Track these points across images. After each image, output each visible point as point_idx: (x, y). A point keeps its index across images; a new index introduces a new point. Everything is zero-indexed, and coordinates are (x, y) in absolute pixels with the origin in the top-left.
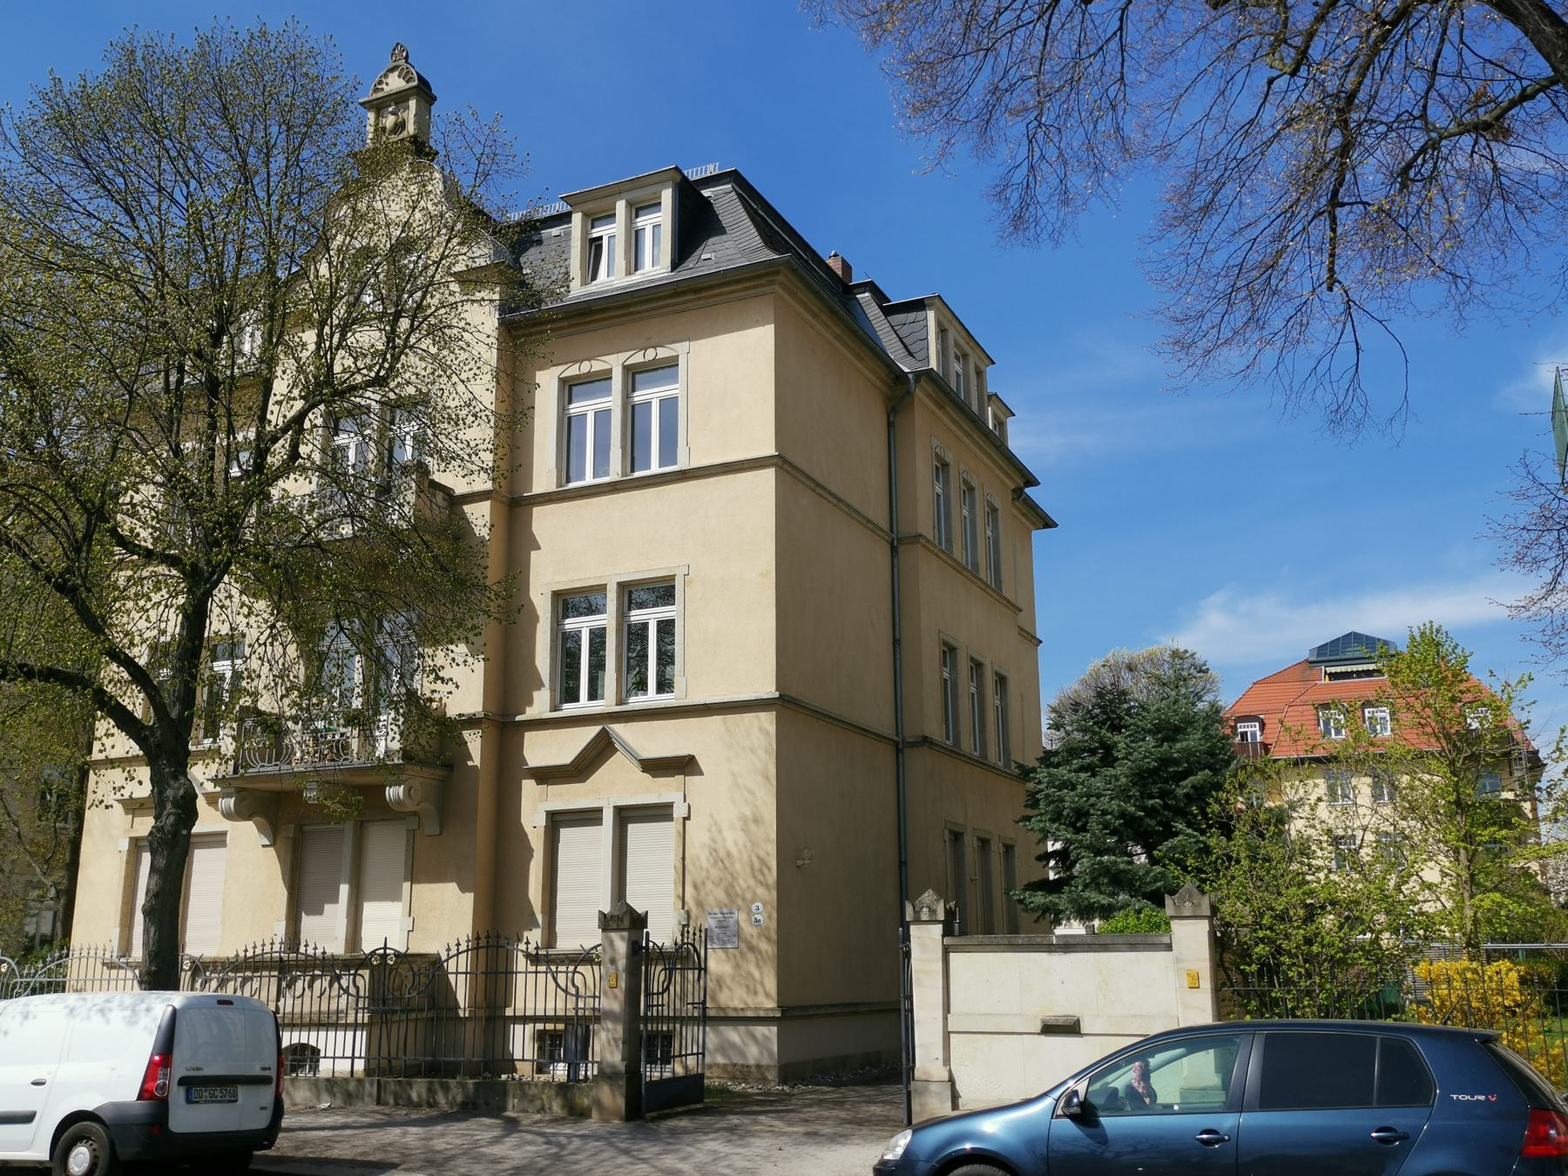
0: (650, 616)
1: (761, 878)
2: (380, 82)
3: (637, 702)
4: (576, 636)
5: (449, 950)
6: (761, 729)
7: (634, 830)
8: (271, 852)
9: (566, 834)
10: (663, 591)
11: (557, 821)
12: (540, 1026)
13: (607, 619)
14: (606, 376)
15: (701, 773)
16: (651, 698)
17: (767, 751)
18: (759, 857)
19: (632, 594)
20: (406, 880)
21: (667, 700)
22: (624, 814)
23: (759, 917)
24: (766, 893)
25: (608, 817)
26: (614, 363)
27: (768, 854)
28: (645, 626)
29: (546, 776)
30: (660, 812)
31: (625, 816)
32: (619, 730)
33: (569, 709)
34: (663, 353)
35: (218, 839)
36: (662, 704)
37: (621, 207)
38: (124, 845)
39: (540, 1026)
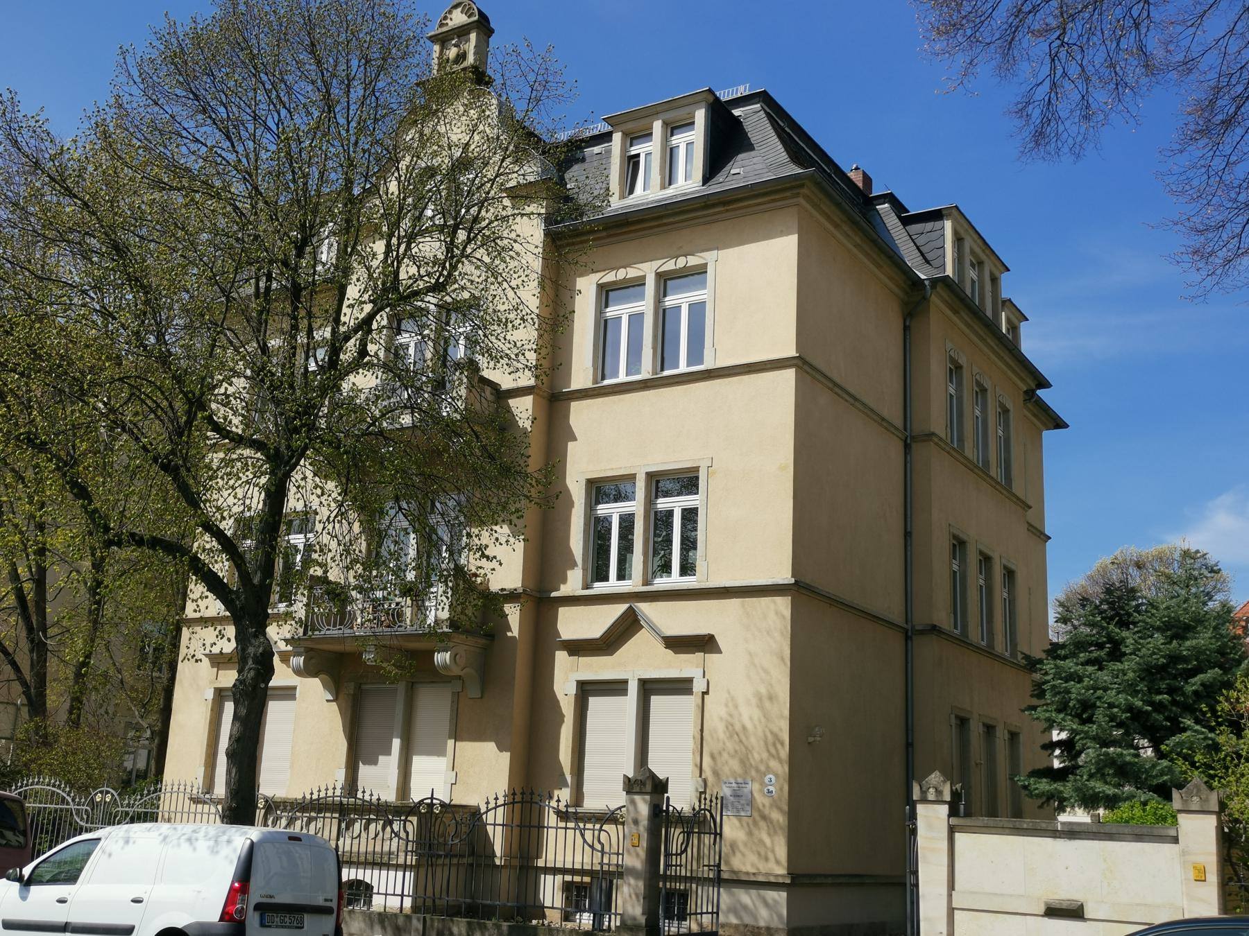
0: (675, 504)
3: (661, 583)
10: (688, 481)
11: (586, 690)
12: (568, 878)
13: (635, 506)
14: (640, 282)
16: (674, 580)
18: (772, 733)
19: (659, 483)
20: (450, 738)
22: (648, 686)
23: (771, 788)
25: (633, 688)
26: (648, 270)
28: (670, 513)
29: (578, 648)
30: (680, 686)
31: (649, 688)
32: (644, 608)
34: (693, 261)
37: (657, 126)
38: (210, 694)
39: (568, 878)
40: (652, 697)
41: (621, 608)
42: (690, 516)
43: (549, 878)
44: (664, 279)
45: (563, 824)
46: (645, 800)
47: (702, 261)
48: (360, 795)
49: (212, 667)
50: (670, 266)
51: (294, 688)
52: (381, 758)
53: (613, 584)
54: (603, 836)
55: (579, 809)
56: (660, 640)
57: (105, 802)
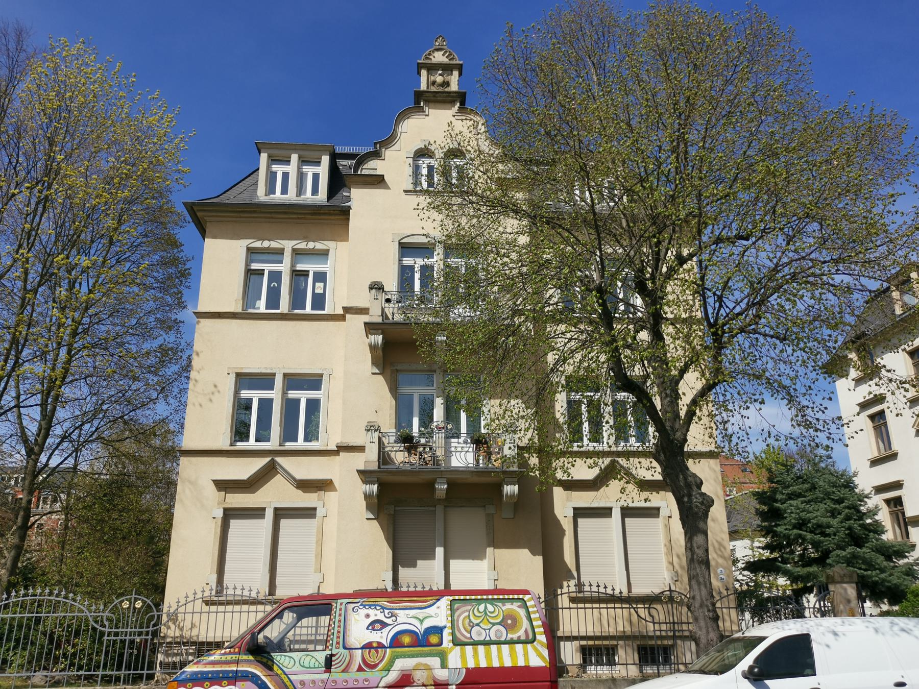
0: (303, 396)
1: (720, 553)
2: (430, 54)
3: (289, 445)
4: (297, 401)
5: (195, 594)
6: (710, 468)
7: (284, 522)
8: (375, 523)
9: (234, 524)
10: (313, 382)
11: (580, 513)
12: (584, 643)
13: (275, 395)
14: (281, 252)
15: (335, 490)
16: (300, 443)
17: (715, 481)
18: (717, 541)
19: (294, 381)
20: (489, 546)
21: (313, 445)
22: (278, 512)
23: (723, 577)
24: (725, 562)
25: (269, 514)
26: (288, 245)
27: (723, 539)
28: (251, 400)
29: (572, 485)
30: (308, 513)
31: (280, 513)
32: (279, 460)
33: (241, 445)
34: (319, 246)
35: (312, 512)
36: (304, 448)
37: (294, 158)
38: (220, 513)
39: (584, 643)
40: (282, 520)
41: (267, 460)
42: (314, 406)
43: (568, 644)
44: (296, 253)
45: (575, 606)
46: (851, 587)
47: (325, 248)
48: (587, 588)
49: (219, 491)
50: (302, 245)
51: (315, 509)
52: (419, 562)
53: (251, 443)
54: (653, 612)
55: (275, 597)
56: (293, 482)
57: (135, 608)
